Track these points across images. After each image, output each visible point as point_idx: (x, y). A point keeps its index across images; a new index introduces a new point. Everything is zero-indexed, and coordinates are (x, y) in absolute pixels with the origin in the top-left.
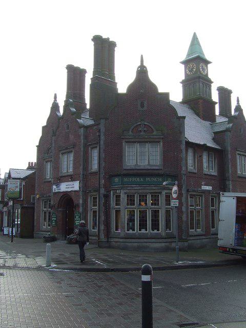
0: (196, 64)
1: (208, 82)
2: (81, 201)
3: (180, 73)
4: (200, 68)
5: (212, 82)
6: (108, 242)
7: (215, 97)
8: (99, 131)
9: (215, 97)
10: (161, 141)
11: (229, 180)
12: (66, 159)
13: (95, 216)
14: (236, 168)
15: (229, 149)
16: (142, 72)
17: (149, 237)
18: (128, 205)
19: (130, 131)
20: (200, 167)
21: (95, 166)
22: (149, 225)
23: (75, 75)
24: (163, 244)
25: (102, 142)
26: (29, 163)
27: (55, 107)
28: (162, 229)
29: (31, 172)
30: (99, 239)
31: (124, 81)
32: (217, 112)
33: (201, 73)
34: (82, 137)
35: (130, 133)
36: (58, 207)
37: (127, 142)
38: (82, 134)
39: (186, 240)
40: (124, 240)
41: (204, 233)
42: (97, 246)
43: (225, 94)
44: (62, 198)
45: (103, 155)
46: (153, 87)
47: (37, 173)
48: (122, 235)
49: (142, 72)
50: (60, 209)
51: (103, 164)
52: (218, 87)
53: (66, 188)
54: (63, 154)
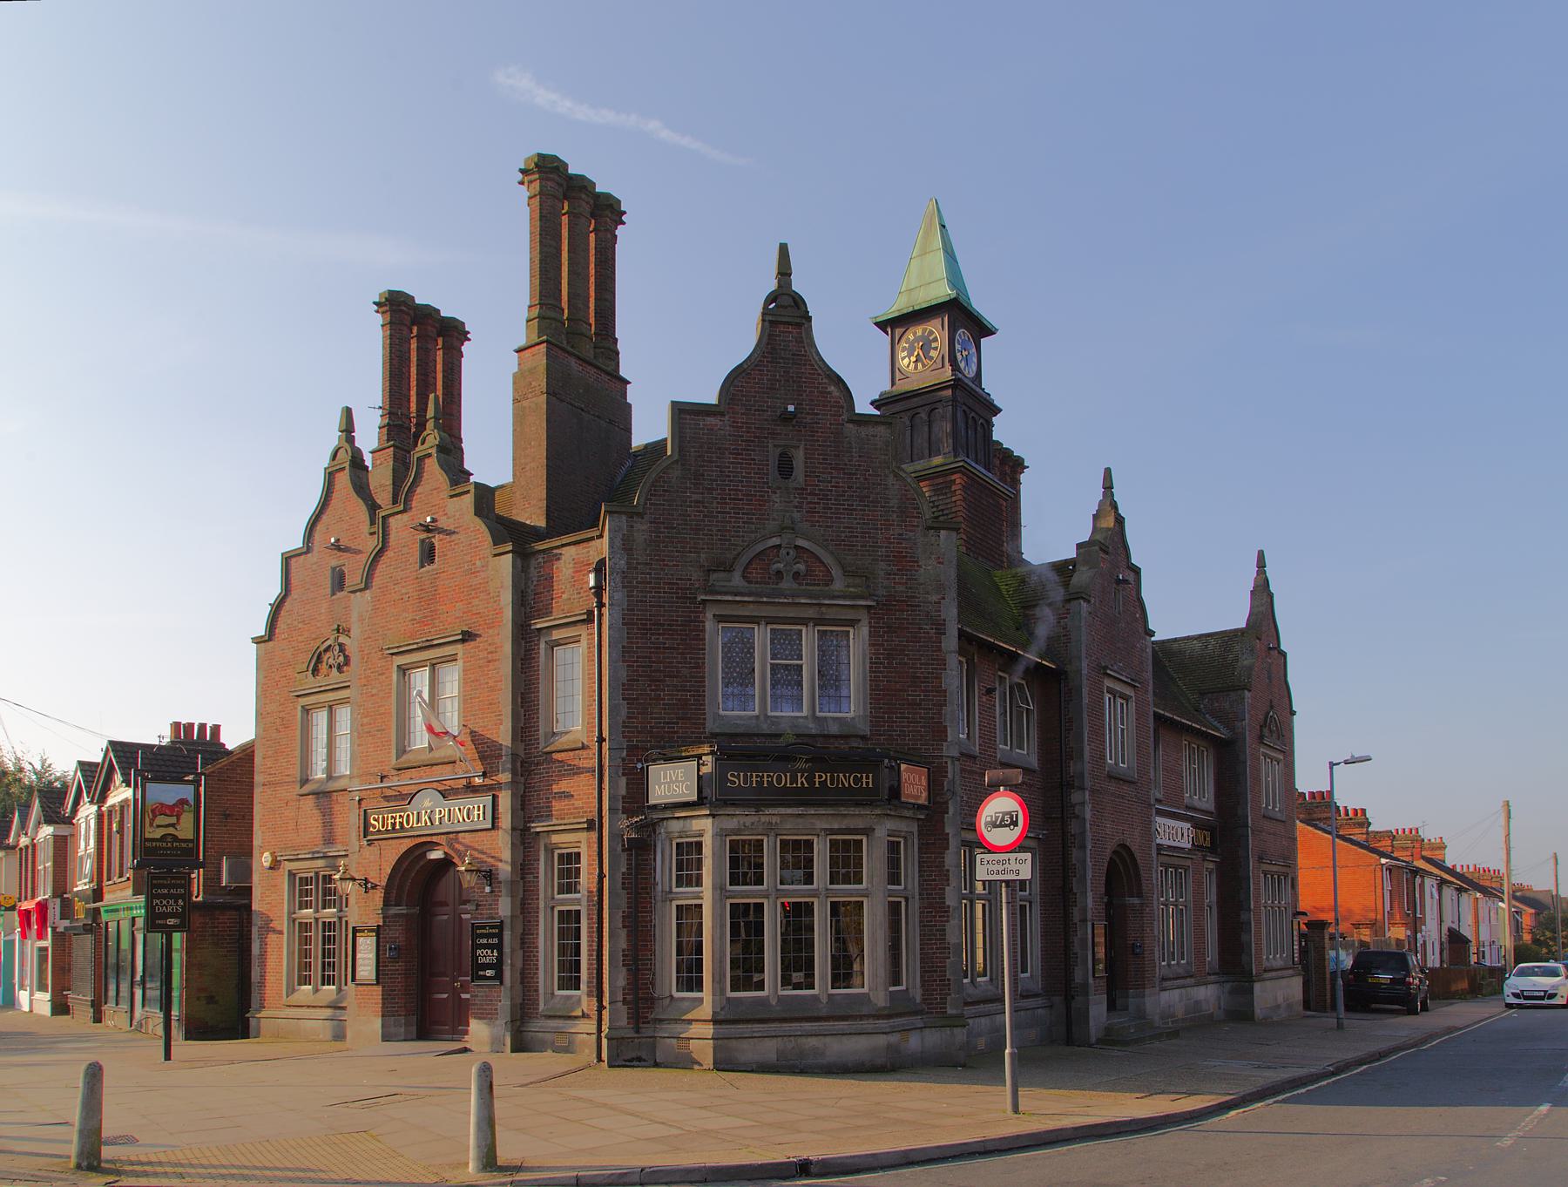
0: (43, 762)
5: (997, 411)
10: (865, 622)
11: (1083, 789)
17: (824, 1013)
23: (421, 341)
24: (881, 1041)
31: (675, 357)
35: (737, 580)
37: (720, 619)
39: (958, 1021)
53: (316, 888)
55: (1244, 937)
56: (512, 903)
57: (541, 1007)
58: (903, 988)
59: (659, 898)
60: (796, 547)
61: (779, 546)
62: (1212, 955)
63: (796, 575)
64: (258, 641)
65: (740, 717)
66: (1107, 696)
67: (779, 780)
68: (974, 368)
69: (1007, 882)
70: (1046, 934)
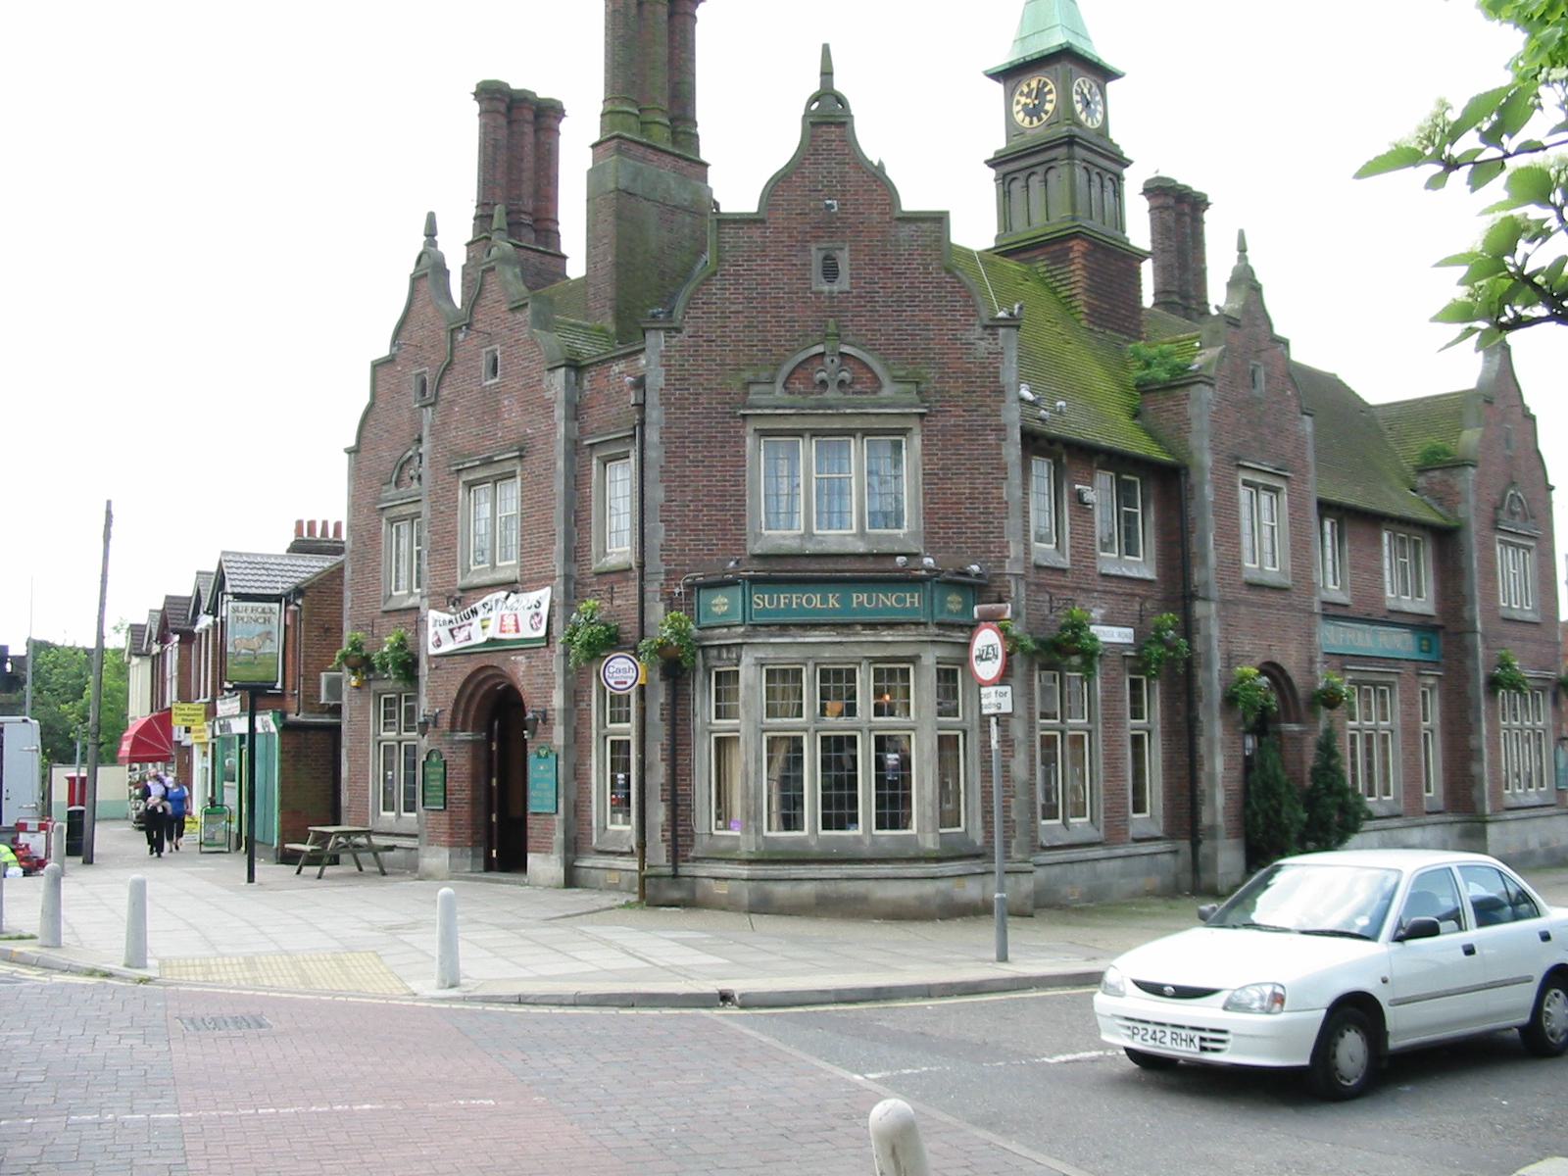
1: (1106, 161)
2: (558, 700)
3: (987, 121)
4: (1076, 98)
6: (675, 876)
7: (1139, 228)
8: (640, 384)
9: (1139, 228)
12: (485, 510)
13: (620, 763)
14: (1238, 545)
15: (1208, 460)
16: (828, 118)
18: (771, 712)
19: (779, 385)
20: (1083, 551)
21: (618, 546)
22: (867, 801)
23: (516, 125)
25: (653, 435)
26: (299, 524)
27: (429, 271)
28: (922, 816)
29: (315, 565)
30: (642, 867)
31: (742, 153)
32: (1148, 300)
33: (1079, 124)
34: (559, 412)
36: (453, 729)
37: (764, 433)
38: (561, 396)
40: (760, 871)
41: (1100, 835)
42: (634, 898)
43: (1180, 209)
44: (471, 687)
45: (657, 494)
46: (877, 180)
47: (347, 574)
48: (748, 845)
49: (828, 118)
50: (461, 736)
51: (658, 534)
52: (1148, 182)
54: (470, 485)
55: (1475, 768)
56: (565, 732)
57: (595, 840)
58: (961, 830)
59: (698, 730)
60: (842, 354)
61: (822, 354)
62: (1434, 793)
63: (842, 383)
64: (349, 451)
65: (784, 537)
66: (1244, 493)
67: (809, 600)
68: (1099, 117)
69: (994, 715)
70: (1169, 766)
